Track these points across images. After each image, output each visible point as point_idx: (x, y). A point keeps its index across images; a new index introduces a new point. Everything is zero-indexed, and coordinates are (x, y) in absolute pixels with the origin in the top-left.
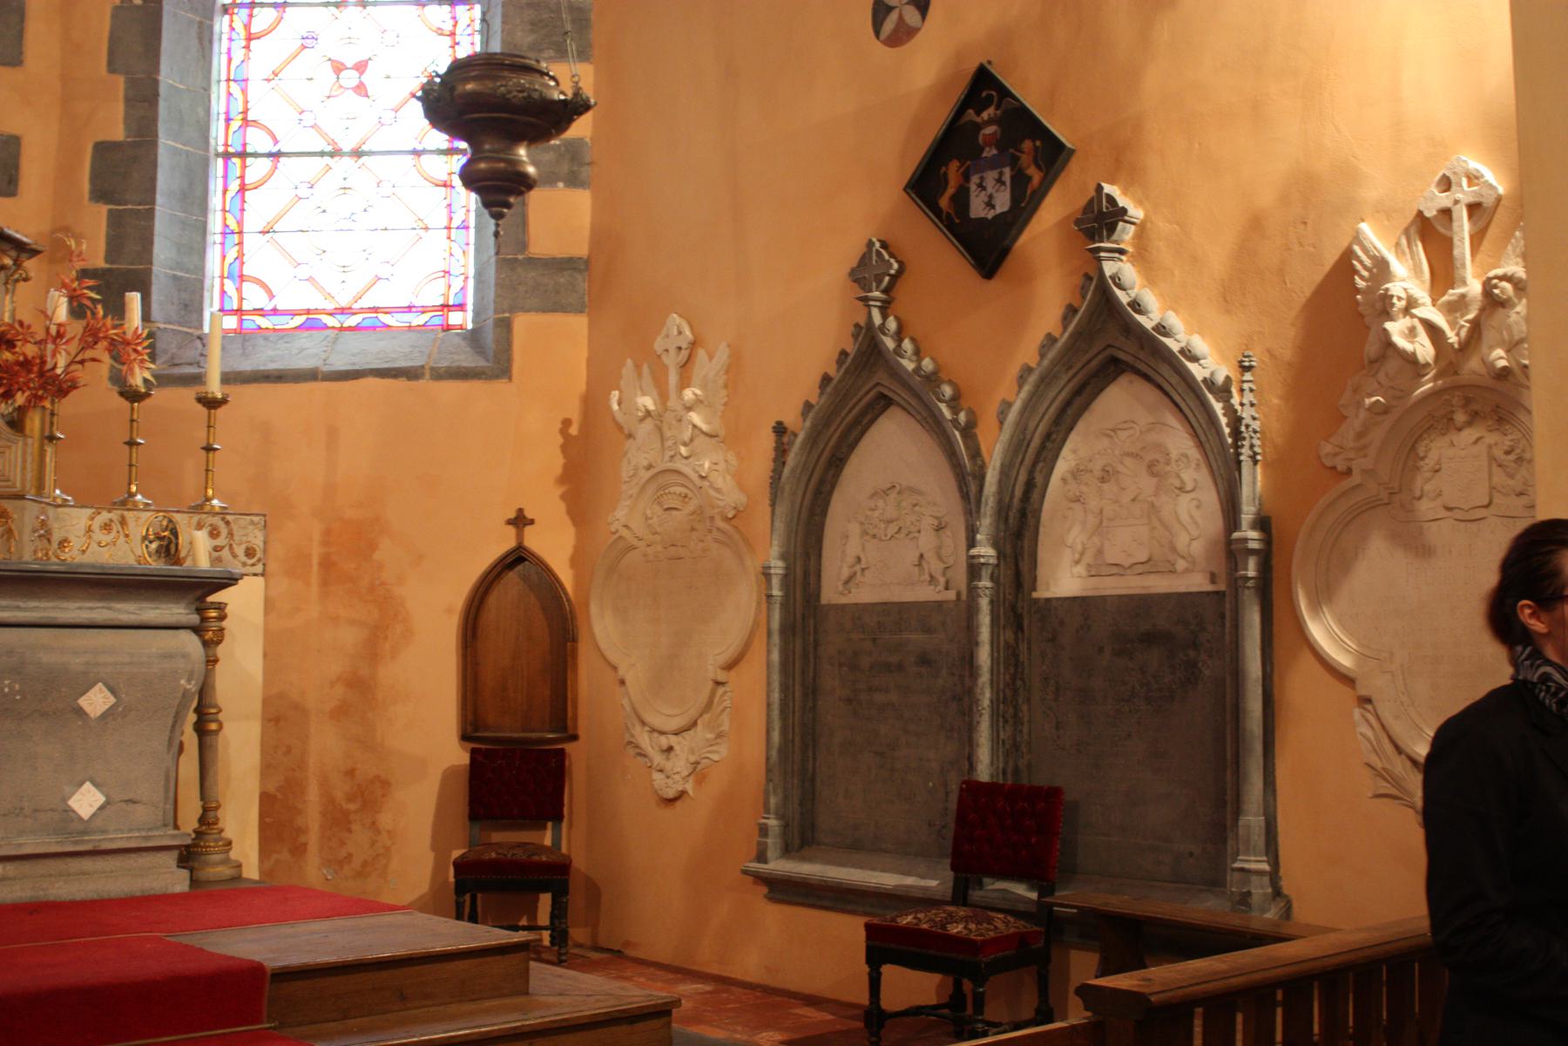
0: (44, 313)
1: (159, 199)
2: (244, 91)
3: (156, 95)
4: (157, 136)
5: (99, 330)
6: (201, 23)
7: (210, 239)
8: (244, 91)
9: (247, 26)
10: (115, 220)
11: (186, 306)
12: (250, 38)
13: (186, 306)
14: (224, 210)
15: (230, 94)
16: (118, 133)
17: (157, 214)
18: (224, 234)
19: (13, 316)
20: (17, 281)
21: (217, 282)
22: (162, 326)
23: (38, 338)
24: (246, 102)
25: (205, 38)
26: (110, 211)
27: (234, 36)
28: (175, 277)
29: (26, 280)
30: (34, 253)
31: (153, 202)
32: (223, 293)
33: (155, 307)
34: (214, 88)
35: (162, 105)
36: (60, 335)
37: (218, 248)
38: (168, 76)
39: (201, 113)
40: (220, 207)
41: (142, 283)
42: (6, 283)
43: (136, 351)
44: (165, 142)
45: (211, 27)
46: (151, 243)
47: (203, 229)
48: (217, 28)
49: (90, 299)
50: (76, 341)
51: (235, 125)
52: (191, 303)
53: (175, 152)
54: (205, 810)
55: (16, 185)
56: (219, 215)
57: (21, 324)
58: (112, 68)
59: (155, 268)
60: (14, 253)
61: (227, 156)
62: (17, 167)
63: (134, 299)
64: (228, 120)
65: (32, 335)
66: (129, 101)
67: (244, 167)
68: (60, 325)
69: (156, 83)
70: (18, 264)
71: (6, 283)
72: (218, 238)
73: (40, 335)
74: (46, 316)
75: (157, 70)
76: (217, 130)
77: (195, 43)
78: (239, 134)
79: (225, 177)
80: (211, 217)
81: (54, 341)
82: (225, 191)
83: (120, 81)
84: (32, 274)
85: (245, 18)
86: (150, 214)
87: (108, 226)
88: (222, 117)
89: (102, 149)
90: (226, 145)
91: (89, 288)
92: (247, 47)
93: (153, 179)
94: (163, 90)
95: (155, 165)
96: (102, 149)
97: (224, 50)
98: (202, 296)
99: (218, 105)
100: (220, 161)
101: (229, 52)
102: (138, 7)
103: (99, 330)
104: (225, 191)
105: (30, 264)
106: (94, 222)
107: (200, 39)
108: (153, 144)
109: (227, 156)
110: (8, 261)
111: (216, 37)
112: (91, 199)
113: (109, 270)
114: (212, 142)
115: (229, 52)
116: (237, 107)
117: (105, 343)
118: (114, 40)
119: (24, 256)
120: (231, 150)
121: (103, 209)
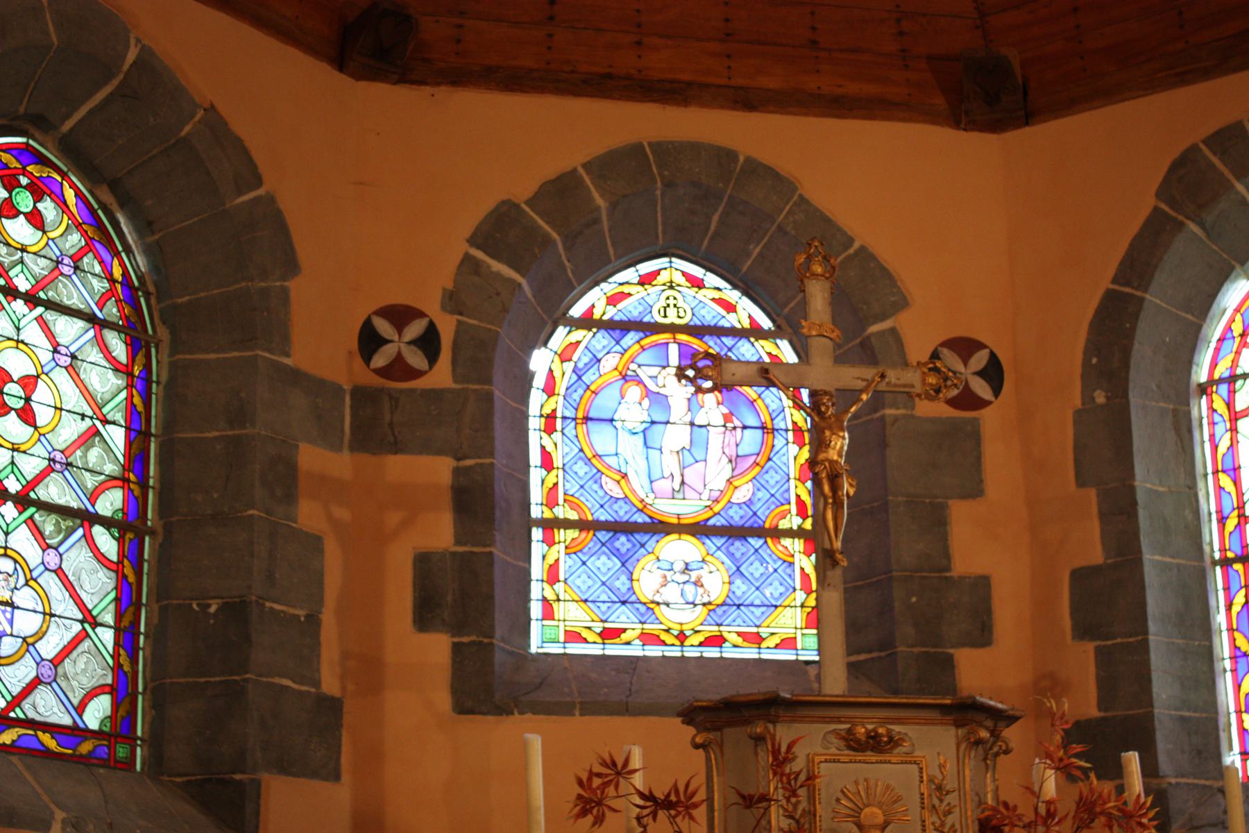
0: (1029, 789)
1: (1152, 627)
2: (1236, 482)
3: (1134, 503)
4: (1140, 552)
5: (1094, 804)
6: (1174, 411)
7: (1218, 667)
8: (1236, 482)
9: (1230, 404)
10: (1103, 657)
11: (1199, 752)
12: (1235, 417)
13: (1199, 752)
14: (1230, 629)
15: (1221, 488)
16: (1096, 555)
17: (1152, 645)
18: (1234, 658)
19: (996, 797)
20: (997, 754)
21: (1233, 718)
22: (1173, 781)
23: (1026, 820)
24: (1240, 494)
25: (1183, 429)
26: (1097, 648)
27: (1217, 418)
28: (1182, 718)
29: (1007, 752)
30: (1011, 719)
31: (1145, 632)
32: (1219, 489)
33: (1162, 758)
34: (1201, 484)
35: (1142, 514)
36: (1050, 815)
37: (1229, 675)
38: (1145, 480)
39: (1190, 517)
40: (1224, 627)
41: (1143, 740)
42: (985, 759)
43: (1141, 824)
44: (1150, 557)
45: (1188, 414)
46: (1149, 681)
47: (1208, 655)
48: (1195, 413)
49: (1079, 768)
50: (1069, 822)
51: (1231, 524)
52: (1204, 733)
53: (1164, 567)
54: (1232, 445)
55: (991, 632)
56: (1225, 635)
57: (1006, 805)
58: (1081, 482)
59: (1156, 711)
60: (990, 723)
61: (1226, 563)
62: (989, 612)
63: (1132, 760)
64: (1222, 520)
65: (1020, 818)
66: (1104, 517)
67: (1232, 392)
68: (1049, 803)
69: (1132, 489)
70: (995, 734)
71: (985, 759)
72: (1228, 664)
73: (1029, 816)
74: (1032, 792)
75: (1131, 475)
76: (1212, 534)
77: (1171, 435)
78: (1236, 536)
79: (1227, 589)
80: (1216, 640)
81: (1045, 824)
82: (1229, 607)
83: (1092, 494)
84: (1012, 745)
85: (1225, 395)
86: (1144, 646)
87: (1097, 667)
88: (1214, 517)
89: (1080, 576)
90: (1223, 550)
91: (1077, 756)
92: (1234, 430)
93: (1142, 605)
94: (1141, 497)
95: (1142, 587)
96: (1080, 576)
97: (1206, 437)
98: (1217, 738)
99: (1209, 505)
100: (1218, 569)
101: (1212, 436)
102: (1102, 406)
103: (1094, 804)
104: (1229, 607)
105: (1012, 734)
106: (1081, 663)
107: (1177, 429)
108: (1138, 562)
109: (1226, 563)
110: (984, 734)
111: (1195, 423)
112: (1074, 638)
113: (1103, 718)
114: (1207, 548)
115: (1212, 436)
116: (1229, 503)
117: (1103, 819)
118: (1079, 448)
119: (1001, 724)
120: (1230, 555)
121: (1090, 647)
